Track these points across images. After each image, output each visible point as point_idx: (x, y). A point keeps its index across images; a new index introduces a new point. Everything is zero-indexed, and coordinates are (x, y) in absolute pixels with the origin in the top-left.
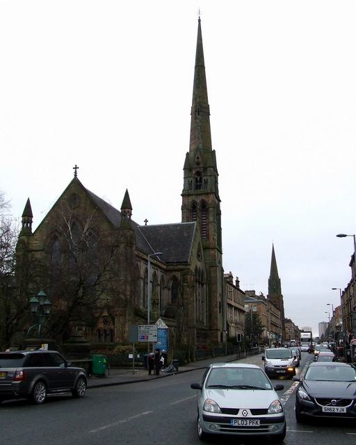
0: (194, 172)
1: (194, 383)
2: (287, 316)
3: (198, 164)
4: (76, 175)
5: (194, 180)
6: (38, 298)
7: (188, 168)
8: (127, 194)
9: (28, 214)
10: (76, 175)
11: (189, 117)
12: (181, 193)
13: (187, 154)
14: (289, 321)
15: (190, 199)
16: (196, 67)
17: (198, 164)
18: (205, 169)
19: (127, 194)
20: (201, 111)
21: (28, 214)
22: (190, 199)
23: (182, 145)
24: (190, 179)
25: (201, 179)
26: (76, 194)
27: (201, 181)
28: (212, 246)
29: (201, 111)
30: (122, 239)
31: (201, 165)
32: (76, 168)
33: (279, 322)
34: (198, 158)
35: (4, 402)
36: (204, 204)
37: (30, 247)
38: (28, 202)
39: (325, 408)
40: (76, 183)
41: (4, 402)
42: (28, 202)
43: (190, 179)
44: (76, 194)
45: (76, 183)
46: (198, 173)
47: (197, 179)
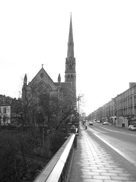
6: (134, 156)
7: (67, 63)
8: (59, 75)
9: (26, 78)
11: (67, 46)
13: (66, 59)
15: (68, 74)
17: (70, 62)
18: (73, 64)
19: (59, 75)
20: (71, 44)
21: (26, 78)
22: (68, 74)
23: (65, 55)
24: (68, 67)
25: (71, 67)
26: (42, 73)
29: (71, 44)
30: (59, 89)
33: (72, 108)
37: (27, 90)
38: (26, 75)
39: (73, 136)
40: (42, 69)
42: (26, 75)
44: (42, 73)
45: (42, 69)
46: (70, 65)
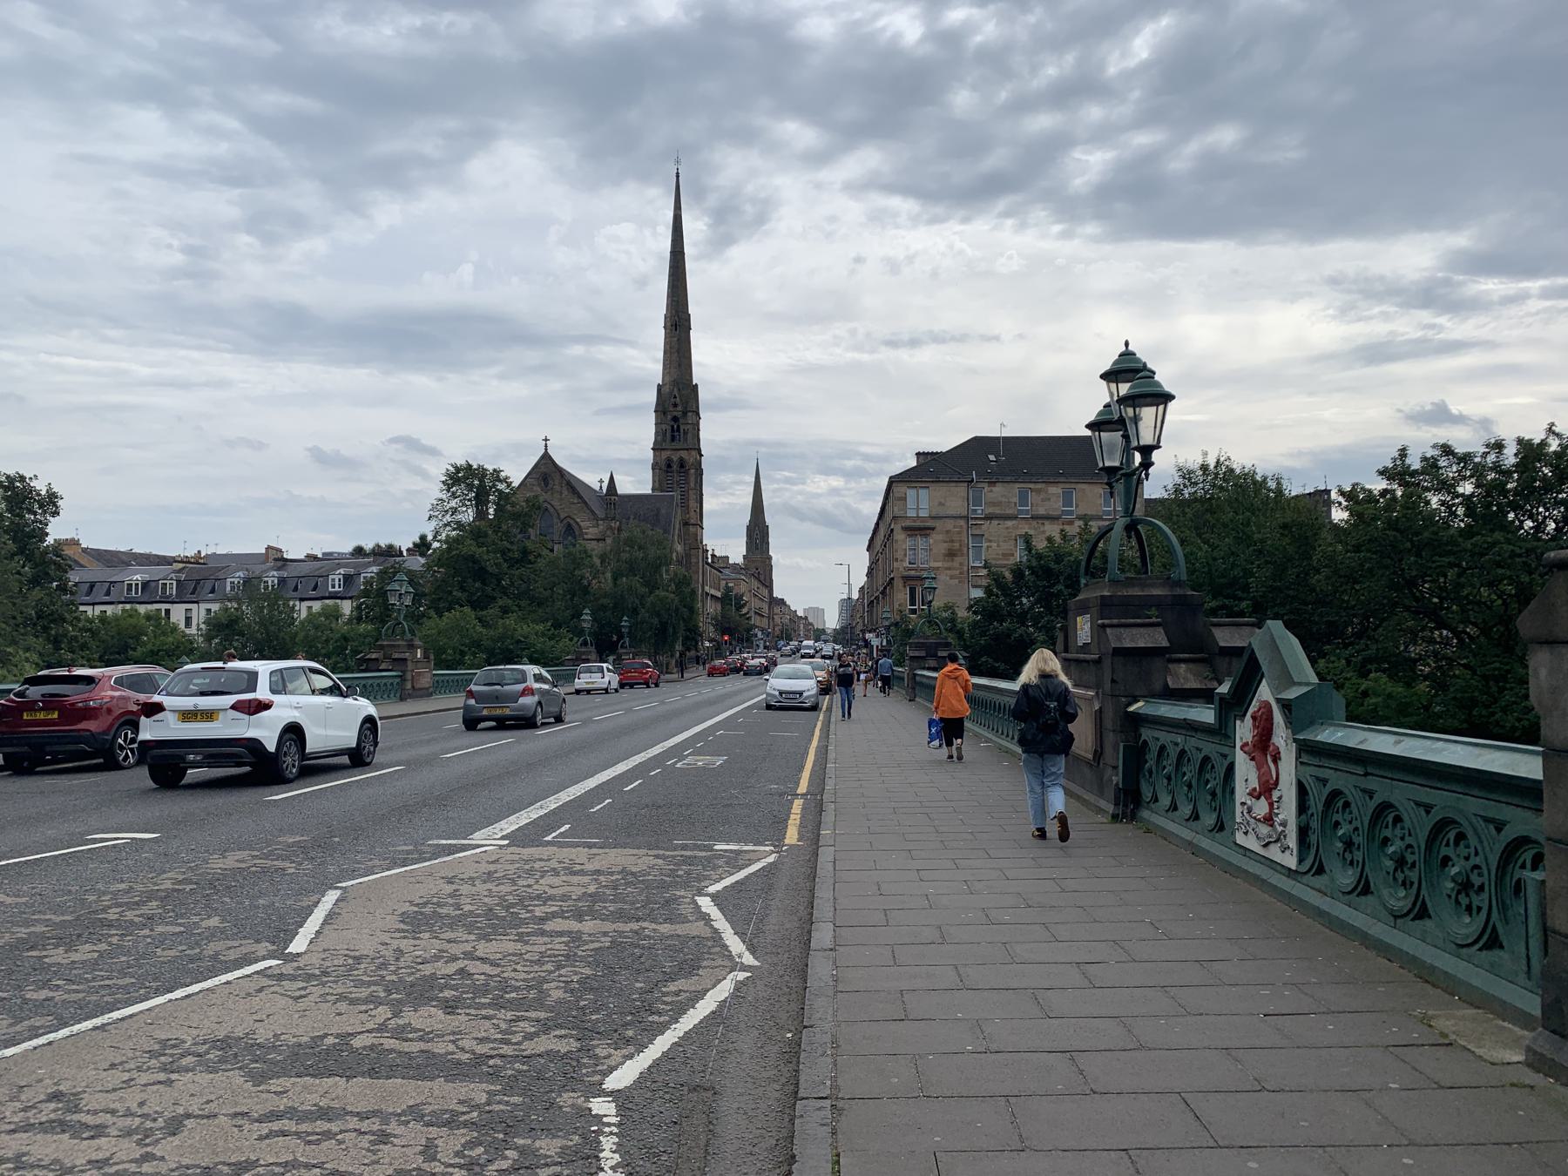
0: (669, 417)
1: (1380, 467)
2: (778, 593)
3: (675, 405)
4: (546, 449)
5: (669, 428)
10: (546, 449)
12: (652, 446)
14: (782, 602)
15: (665, 454)
16: (672, 252)
18: (685, 414)
22: (665, 454)
24: (664, 427)
25: (678, 427)
27: (678, 430)
28: (692, 521)
31: (679, 408)
32: (546, 440)
34: (675, 397)
35: (38, 769)
36: (682, 463)
40: (546, 457)
41: (38, 769)
43: (664, 427)
45: (546, 457)
46: (675, 419)
47: (673, 427)
